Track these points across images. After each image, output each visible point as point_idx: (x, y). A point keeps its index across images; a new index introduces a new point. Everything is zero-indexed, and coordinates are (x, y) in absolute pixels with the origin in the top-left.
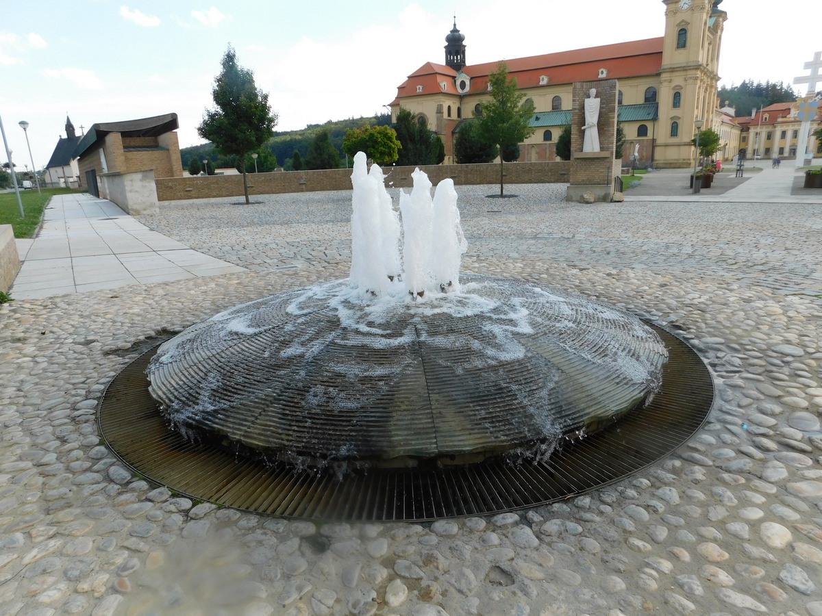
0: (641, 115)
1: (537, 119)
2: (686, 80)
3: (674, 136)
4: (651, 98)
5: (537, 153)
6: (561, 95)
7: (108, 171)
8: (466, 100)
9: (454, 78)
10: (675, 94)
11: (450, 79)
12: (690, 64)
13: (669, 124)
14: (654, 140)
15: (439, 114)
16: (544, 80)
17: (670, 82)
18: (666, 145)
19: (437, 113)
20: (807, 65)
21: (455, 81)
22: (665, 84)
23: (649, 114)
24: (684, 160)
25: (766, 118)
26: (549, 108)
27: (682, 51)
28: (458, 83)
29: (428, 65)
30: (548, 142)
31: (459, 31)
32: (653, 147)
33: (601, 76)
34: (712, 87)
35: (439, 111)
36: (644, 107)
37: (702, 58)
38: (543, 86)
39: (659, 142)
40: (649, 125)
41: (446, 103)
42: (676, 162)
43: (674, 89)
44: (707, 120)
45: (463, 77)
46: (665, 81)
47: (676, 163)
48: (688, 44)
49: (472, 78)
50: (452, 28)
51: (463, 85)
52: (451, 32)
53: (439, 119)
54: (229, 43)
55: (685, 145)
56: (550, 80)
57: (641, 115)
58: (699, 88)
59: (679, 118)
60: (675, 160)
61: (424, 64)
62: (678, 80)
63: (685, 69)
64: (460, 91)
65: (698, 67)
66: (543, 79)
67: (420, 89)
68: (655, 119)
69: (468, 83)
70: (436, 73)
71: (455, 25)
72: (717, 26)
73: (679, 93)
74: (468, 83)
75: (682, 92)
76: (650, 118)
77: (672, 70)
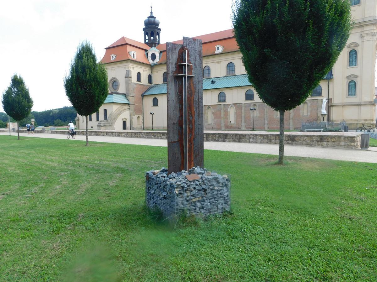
1: (213, 82)
2: (362, 37)
3: (352, 95)
5: (213, 113)
7: (286, 136)
8: (156, 69)
9: (146, 51)
11: (143, 51)
15: (127, 78)
16: (220, 49)
18: (343, 106)
19: (126, 77)
21: (147, 54)
24: (366, 120)
26: (224, 74)
28: (150, 55)
30: (222, 103)
31: (155, 18)
33: (217, 52)
35: (128, 76)
38: (218, 54)
39: (335, 101)
41: (135, 70)
42: (356, 122)
45: (154, 50)
47: (357, 124)
49: (161, 52)
50: (149, 15)
51: (153, 57)
52: (148, 18)
53: (128, 83)
55: (366, 104)
56: (224, 49)
59: (357, 77)
60: (355, 120)
64: (151, 62)
66: (218, 48)
67: (113, 57)
69: (158, 55)
70: (127, 44)
71: (151, 13)
72: (281, 157)
73: (355, 51)
74: (158, 55)
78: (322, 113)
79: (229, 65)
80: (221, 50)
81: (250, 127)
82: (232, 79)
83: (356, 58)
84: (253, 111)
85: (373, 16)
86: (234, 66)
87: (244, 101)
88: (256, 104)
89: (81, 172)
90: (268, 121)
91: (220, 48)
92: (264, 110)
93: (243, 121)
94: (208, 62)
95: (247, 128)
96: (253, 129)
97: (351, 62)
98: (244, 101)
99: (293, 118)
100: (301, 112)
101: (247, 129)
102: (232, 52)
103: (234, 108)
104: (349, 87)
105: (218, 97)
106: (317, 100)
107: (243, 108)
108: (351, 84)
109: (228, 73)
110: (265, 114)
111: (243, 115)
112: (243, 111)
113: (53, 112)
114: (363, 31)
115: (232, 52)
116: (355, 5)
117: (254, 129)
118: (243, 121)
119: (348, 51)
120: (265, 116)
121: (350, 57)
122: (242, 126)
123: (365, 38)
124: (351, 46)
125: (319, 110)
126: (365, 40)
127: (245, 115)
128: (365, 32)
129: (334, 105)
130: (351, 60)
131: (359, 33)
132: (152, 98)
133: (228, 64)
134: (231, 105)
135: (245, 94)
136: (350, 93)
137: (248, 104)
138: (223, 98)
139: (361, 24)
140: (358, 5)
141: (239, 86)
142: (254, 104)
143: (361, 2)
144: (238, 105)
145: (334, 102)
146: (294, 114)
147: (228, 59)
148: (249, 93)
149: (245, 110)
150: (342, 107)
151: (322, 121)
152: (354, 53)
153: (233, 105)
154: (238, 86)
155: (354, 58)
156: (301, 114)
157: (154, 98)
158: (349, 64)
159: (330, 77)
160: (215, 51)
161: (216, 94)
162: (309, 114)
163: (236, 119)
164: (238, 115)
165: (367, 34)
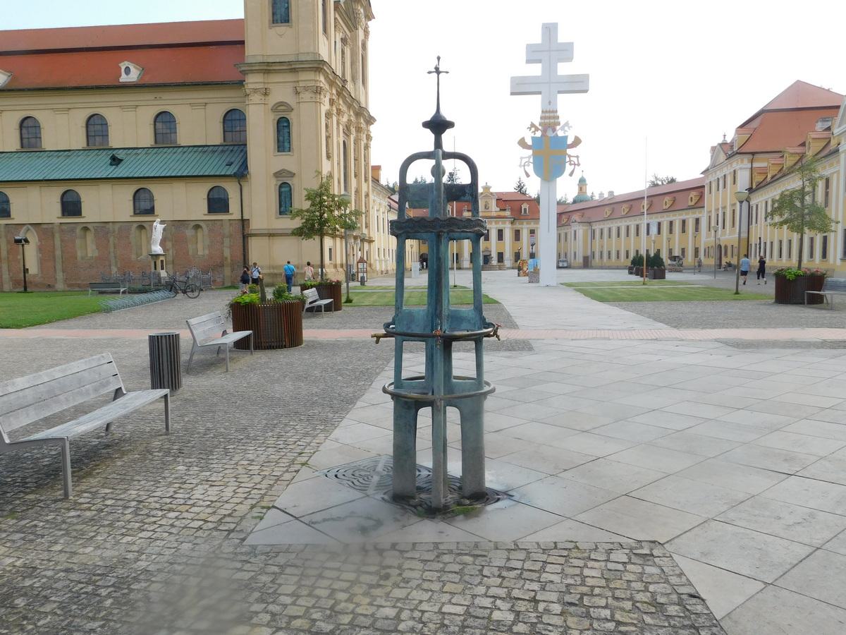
0: (214, 165)
1: (115, 161)
4: (234, 121)
6: (40, 116)
10: (279, 122)
12: (302, 58)
13: (273, 184)
14: (244, 222)
17: (266, 94)
18: (271, 235)
20: (534, 54)
22: (256, 98)
23: (230, 164)
25: (525, 209)
26: (147, 139)
27: (282, 29)
29: (799, 88)
32: (245, 237)
33: (124, 78)
34: (359, 130)
36: (222, 151)
37: (326, 49)
39: (255, 226)
40: (231, 189)
43: (275, 108)
44: (357, 192)
46: (255, 90)
48: (293, 15)
54: (430, 73)
56: (13, 79)
57: (214, 165)
58: (329, 115)
61: (791, 84)
62: (281, 91)
63: (293, 67)
65: (318, 66)
66: (128, 71)
68: (242, 174)
73: (288, 121)
75: (292, 117)
76: (232, 170)
77: (268, 68)
78: (153, 253)
79: (160, 117)
80: (134, 76)
81: (78, 282)
82: (32, 160)
83: (289, 136)
84: (23, 245)
85: (314, 53)
86: (107, 124)
87: (58, 218)
88: (89, 226)
89: (455, 508)
90: (118, 269)
91: (132, 69)
92: (109, 242)
93: (59, 266)
94: (32, 107)
95: (70, 285)
96: (25, 289)
97: (281, 144)
98: (58, 218)
99: (173, 261)
100: (191, 247)
101: (69, 289)
102: (29, 90)
103: (35, 234)
104: (280, 196)
105: (132, 202)
106: (220, 222)
107: (57, 236)
108: (283, 190)
109: (229, 135)
110: (112, 250)
111: (58, 253)
112: (58, 242)
113: (827, 209)
114: (298, 82)
115: (29, 90)
116: (282, 23)
117: (28, 290)
118: (59, 266)
119: (274, 119)
120: (112, 254)
121: (278, 131)
122: (56, 279)
123: (301, 95)
124: (279, 108)
125: (225, 245)
126: (302, 100)
127: (62, 252)
128: (301, 84)
129: (253, 232)
130: (281, 138)
131: (292, 84)
132: (133, 188)
133: (155, 114)
134: (25, 227)
135: (206, 197)
136: (282, 209)
137: (68, 225)
138: (144, 205)
139: (293, 67)
140: (287, 24)
141: (42, 180)
142: (85, 225)
143: (292, 20)
144: (45, 226)
145: (254, 228)
146: (175, 252)
147: (91, 105)
148: (68, 198)
149: (62, 241)
150: (267, 238)
151: (153, 270)
152: (285, 124)
153: (30, 227)
154: (41, 178)
155: (287, 134)
156: (190, 253)
157: (138, 191)
158: (278, 147)
159: (242, 173)
160: (121, 76)
161: (127, 192)
162: (207, 252)
163: (42, 262)
164: (46, 255)
165: (306, 89)
